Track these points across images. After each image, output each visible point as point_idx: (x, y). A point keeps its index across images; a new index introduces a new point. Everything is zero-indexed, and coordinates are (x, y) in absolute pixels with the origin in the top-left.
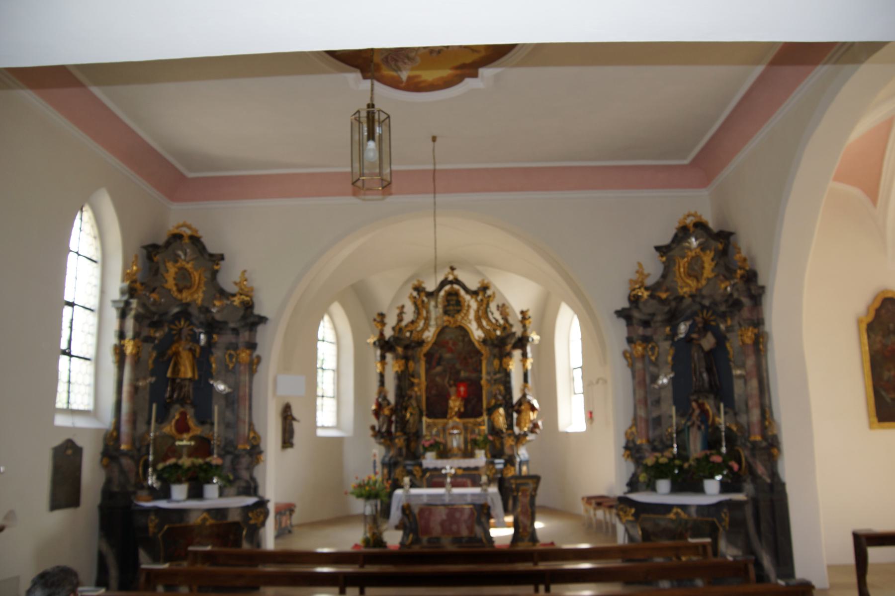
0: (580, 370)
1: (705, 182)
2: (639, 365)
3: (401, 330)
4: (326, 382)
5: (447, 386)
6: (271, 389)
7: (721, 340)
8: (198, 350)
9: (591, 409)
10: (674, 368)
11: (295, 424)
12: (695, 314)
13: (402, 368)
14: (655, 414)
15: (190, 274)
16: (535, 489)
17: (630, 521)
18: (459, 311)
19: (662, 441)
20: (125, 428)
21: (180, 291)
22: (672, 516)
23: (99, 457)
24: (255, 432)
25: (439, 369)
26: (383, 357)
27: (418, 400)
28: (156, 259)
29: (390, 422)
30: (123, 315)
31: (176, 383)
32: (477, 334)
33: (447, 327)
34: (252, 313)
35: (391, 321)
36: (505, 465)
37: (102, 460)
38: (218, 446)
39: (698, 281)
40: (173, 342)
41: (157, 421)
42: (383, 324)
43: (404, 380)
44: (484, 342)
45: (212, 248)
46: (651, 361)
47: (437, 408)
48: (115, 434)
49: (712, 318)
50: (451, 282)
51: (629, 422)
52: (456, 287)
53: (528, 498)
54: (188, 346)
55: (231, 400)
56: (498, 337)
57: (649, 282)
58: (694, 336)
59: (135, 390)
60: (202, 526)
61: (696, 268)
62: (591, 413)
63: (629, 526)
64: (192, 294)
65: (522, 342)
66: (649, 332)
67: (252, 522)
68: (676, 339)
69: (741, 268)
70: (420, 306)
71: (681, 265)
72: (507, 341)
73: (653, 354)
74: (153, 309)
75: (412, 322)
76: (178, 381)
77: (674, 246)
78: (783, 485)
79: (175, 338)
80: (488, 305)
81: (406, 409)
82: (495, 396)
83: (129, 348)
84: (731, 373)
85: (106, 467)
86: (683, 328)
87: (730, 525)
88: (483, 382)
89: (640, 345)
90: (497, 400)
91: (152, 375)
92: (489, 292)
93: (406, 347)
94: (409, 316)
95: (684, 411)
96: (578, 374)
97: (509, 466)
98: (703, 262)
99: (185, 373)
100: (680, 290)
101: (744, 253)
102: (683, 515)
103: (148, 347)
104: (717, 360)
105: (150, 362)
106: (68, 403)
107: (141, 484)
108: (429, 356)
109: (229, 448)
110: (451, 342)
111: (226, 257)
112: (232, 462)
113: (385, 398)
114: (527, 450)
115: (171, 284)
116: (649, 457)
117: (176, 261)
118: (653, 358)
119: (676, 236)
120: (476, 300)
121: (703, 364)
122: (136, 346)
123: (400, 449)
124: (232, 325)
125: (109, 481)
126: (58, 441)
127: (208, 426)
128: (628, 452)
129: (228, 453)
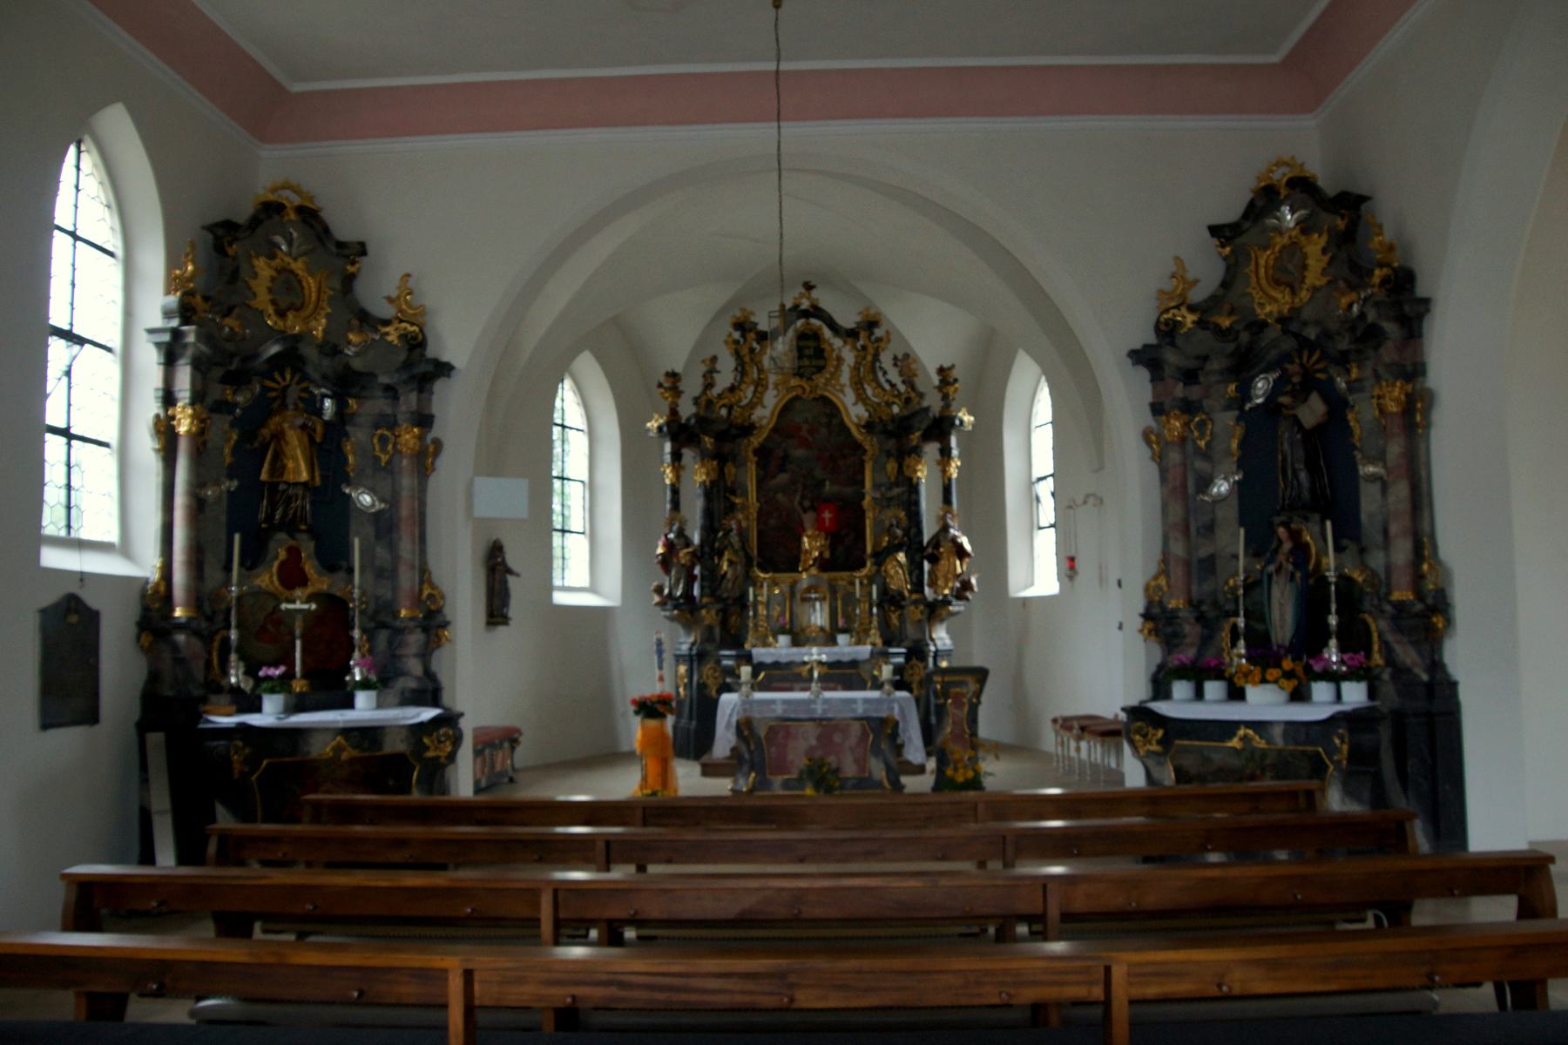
0: (1051, 480)
1: (1307, 105)
2: (1175, 457)
3: (710, 403)
4: (571, 504)
5: (799, 509)
6: (462, 505)
7: (1338, 407)
8: (319, 429)
9: (1072, 553)
10: (1241, 465)
11: (511, 580)
12: (1286, 357)
13: (714, 476)
14: (1203, 552)
15: (300, 282)
16: (978, 694)
17: (1154, 753)
18: (820, 369)
19: (1215, 604)
20: (179, 577)
21: (281, 314)
22: (1235, 743)
23: (133, 630)
24: (433, 587)
25: (783, 478)
26: (676, 456)
27: (743, 534)
28: (230, 252)
29: (691, 579)
30: (170, 355)
31: (275, 491)
32: (854, 412)
33: (797, 398)
34: (423, 355)
35: (692, 386)
36: (908, 656)
37: (138, 638)
38: (362, 612)
39: (1293, 293)
40: (271, 414)
41: (242, 564)
42: (676, 391)
43: (719, 497)
44: (869, 426)
45: (344, 230)
46: (1198, 448)
47: (778, 554)
48: (162, 588)
49: (1321, 366)
50: (806, 314)
51: (1153, 568)
52: (815, 322)
53: (966, 708)
54: (300, 421)
55: (384, 525)
56: (893, 418)
57: (1197, 295)
58: (1284, 400)
59: (198, 506)
60: (334, 761)
61: (1290, 267)
62: (1072, 560)
63: (1150, 763)
64: (306, 320)
65: (941, 428)
66: (1195, 392)
67: (430, 754)
68: (1248, 406)
69: (1381, 265)
70: (747, 359)
71: (1262, 262)
72: (917, 424)
73: (1202, 437)
74: (230, 347)
75: (732, 389)
76: (282, 487)
77: (1247, 225)
78: (1453, 685)
79: (275, 405)
80: (876, 357)
81: (721, 556)
82: (889, 531)
83: (183, 427)
84: (1357, 470)
85: (148, 651)
86: (1261, 386)
87: (1350, 759)
88: (866, 502)
89: (1177, 418)
90: (893, 536)
91: (231, 477)
92: (878, 332)
93: (721, 437)
94: (725, 378)
95: (1260, 546)
96: (1045, 489)
97: (914, 661)
98: (1305, 256)
99: (297, 471)
100: (1258, 311)
101: (1388, 235)
102: (1260, 743)
103: (221, 423)
104: (1330, 448)
105: (227, 451)
106: (69, 527)
107: (215, 686)
108: (763, 453)
109: (381, 618)
110: (805, 427)
111: (370, 249)
112: (390, 642)
113: (681, 533)
114: (948, 632)
115: (262, 300)
116: (1186, 630)
117: (272, 256)
118: (1202, 443)
119: (1251, 204)
120: (854, 347)
121: (1300, 453)
122: (200, 420)
123: (710, 628)
124: (384, 379)
125: (154, 678)
126: (50, 597)
127: (341, 575)
128: (1150, 625)
129: (384, 625)
